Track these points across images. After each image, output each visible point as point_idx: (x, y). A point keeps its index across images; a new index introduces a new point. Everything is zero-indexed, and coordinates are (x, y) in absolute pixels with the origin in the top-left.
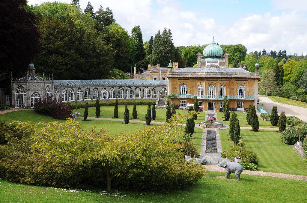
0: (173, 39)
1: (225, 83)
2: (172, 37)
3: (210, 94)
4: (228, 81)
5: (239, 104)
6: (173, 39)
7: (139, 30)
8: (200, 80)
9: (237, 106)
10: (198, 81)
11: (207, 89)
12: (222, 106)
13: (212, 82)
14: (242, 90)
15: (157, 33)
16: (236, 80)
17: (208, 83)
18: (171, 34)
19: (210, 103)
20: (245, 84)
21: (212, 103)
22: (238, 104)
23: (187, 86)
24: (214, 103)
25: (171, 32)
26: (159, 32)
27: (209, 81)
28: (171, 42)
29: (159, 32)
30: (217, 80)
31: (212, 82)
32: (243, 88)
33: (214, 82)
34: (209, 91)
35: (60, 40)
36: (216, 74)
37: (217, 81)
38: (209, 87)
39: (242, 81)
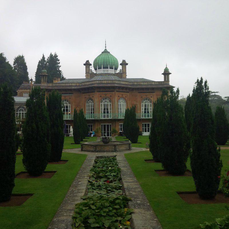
0: (61, 66)
1: (124, 96)
2: (59, 63)
3: (104, 112)
4: (128, 94)
5: (145, 126)
6: (61, 66)
7: (24, 60)
8: (88, 92)
9: (143, 129)
10: (85, 94)
11: (99, 105)
12: (121, 128)
13: (106, 95)
14: (147, 110)
15: (41, 58)
16: (139, 93)
17: (101, 96)
18: (59, 60)
19: (105, 126)
20: (151, 97)
21: (108, 126)
22: (143, 127)
23: (70, 104)
24: (110, 125)
25: (59, 58)
26: (44, 58)
27: (102, 93)
28: (58, 69)
29: (44, 58)
30: (113, 91)
31: (106, 95)
32: (109, 103)
33: (109, 94)
34: (102, 108)
35: (105, 184)
36: (111, 82)
37: (114, 92)
38: (102, 102)
39: (148, 94)
